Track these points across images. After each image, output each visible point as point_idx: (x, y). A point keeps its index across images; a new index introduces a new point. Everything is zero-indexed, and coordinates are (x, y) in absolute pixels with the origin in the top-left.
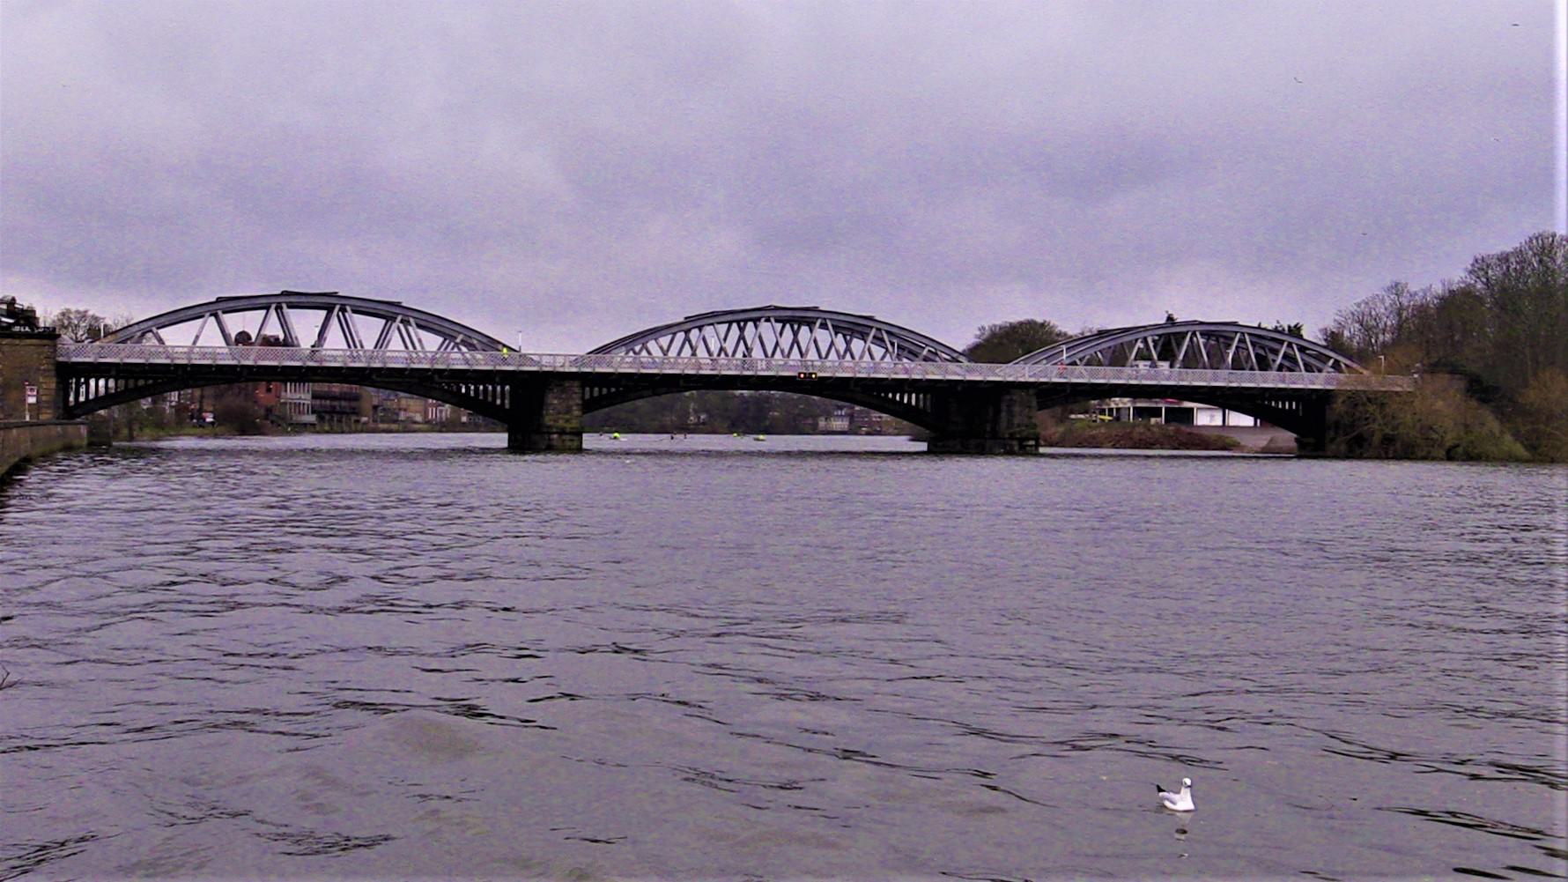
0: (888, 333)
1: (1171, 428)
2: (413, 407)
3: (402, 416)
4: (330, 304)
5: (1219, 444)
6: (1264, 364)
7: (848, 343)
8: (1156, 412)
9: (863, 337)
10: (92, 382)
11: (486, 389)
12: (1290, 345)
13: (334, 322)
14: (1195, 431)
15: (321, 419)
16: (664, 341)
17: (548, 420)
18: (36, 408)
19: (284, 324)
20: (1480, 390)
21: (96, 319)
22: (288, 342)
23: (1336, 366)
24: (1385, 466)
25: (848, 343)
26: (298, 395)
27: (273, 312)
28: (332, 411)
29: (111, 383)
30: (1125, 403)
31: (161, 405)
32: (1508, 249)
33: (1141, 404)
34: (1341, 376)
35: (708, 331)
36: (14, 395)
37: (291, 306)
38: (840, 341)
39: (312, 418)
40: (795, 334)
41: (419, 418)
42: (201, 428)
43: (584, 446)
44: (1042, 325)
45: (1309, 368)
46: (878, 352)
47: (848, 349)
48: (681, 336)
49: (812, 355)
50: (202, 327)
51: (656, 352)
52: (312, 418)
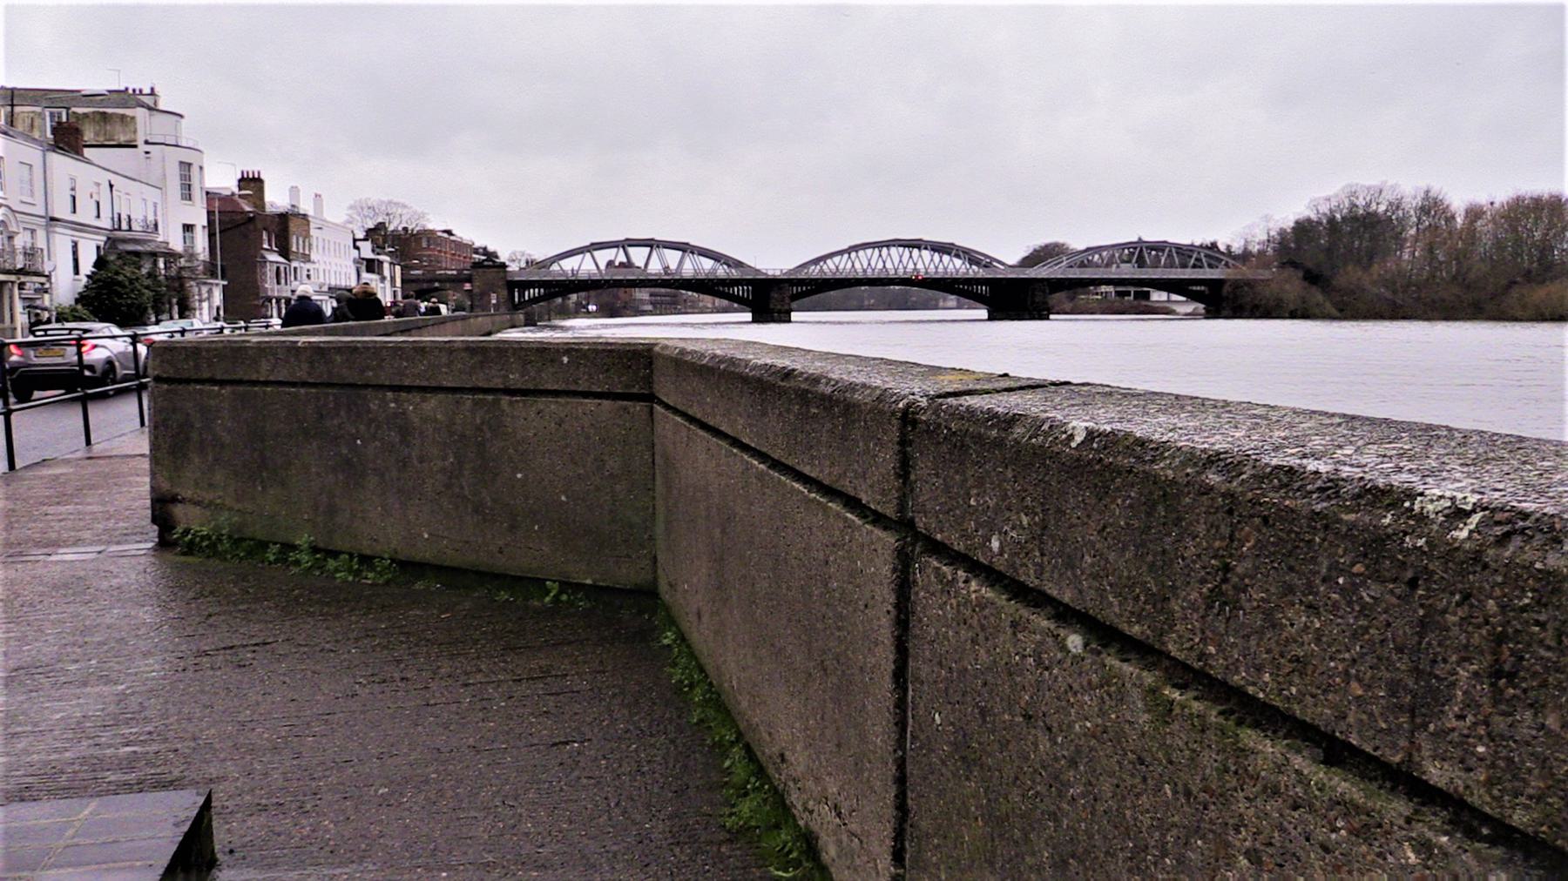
0: (963, 252)
1: (1136, 302)
2: (707, 300)
3: (701, 304)
4: (651, 244)
5: (1164, 311)
6: (1184, 266)
7: (941, 257)
8: (1128, 293)
9: (949, 254)
10: (532, 291)
11: (748, 289)
12: (1199, 253)
13: (654, 253)
14: (1149, 304)
15: (655, 307)
17: (772, 306)
18: (497, 307)
20: (1313, 278)
21: (530, 255)
22: (628, 265)
23: (1227, 265)
24: (1556, 329)
26: (642, 294)
27: (621, 250)
28: (662, 303)
29: (542, 290)
30: (1110, 289)
31: (567, 302)
32: (1331, 193)
33: (1120, 289)
34: (1229, 270)
36: (486, 298)
37: (630, 246)
39: (650, 307)
40: (911, 253)
41: (710, 305)
42: (589, 314)
43: (792, 319)
44: (1063, 245)
45: (1210, 266)
46: (958, 262)
48: (846, 256)
50: (583, 258)
52: (650, 307)
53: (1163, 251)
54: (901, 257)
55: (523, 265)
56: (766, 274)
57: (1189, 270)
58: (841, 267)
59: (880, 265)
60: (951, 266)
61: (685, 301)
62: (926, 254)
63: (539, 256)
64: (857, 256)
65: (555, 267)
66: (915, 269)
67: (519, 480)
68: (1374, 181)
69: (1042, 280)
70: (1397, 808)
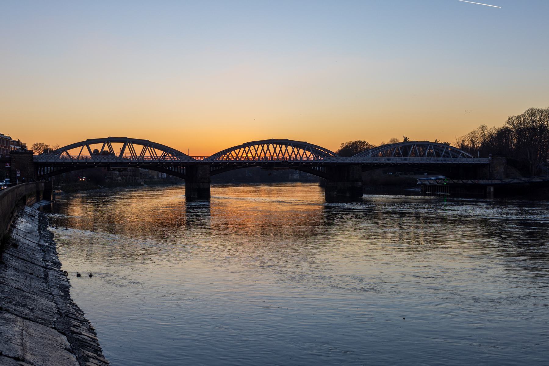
4: (126, 141)
7: (298, 151)
10: (46, 168)
11: (183, 169)
16: (237, 151)
19: (110, 147)
21: (47, 146)
22: (112, 154)
25: (298, 151)
29: (52, 168)
35: (252, 148)
38: (295, 149)
40: (281, 148)
45: (453, 156)
46: (308, 153)
47: (298, 153)
48: (242, 149)
49: (287, 155)
51: (235, 155)
54: (256, 151)
55: (42, 151)
58: (240, 155)
59: (244, 155)
60: (305, 155)
61: (141, 174)
62: (290, 149)
63: (53, 146)
65: (64, 154)
66: (283, 157)
67: (23, 178)
68: (532, 107)
69: (358, 164)
70: (173, 206)
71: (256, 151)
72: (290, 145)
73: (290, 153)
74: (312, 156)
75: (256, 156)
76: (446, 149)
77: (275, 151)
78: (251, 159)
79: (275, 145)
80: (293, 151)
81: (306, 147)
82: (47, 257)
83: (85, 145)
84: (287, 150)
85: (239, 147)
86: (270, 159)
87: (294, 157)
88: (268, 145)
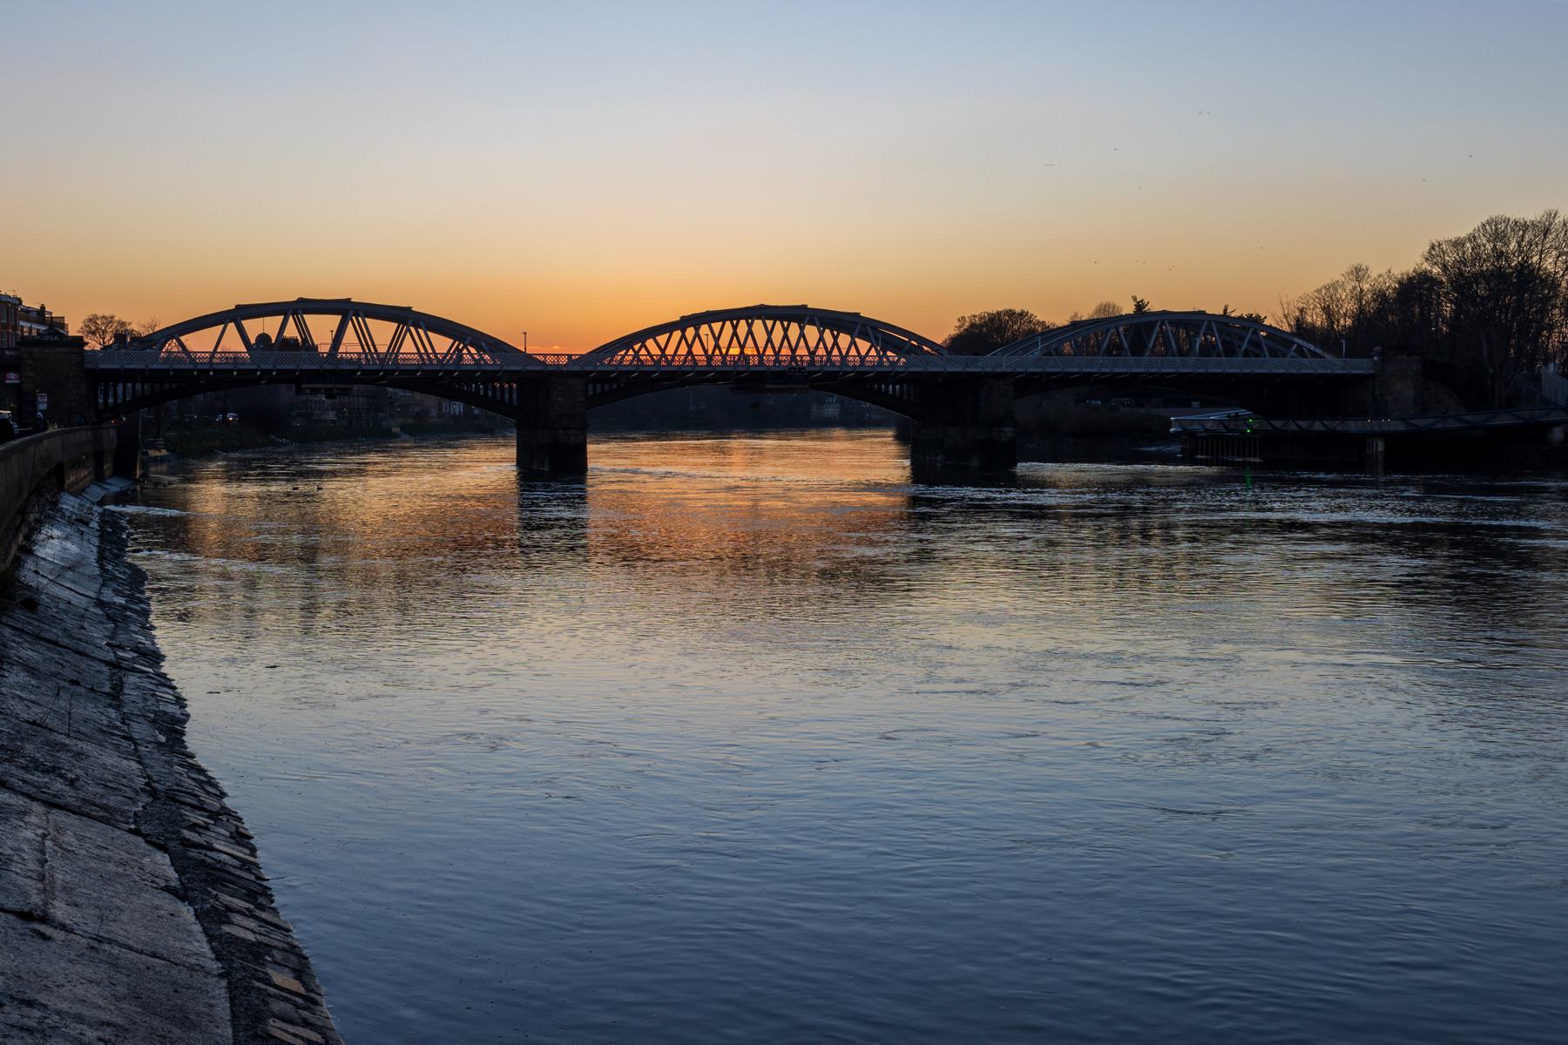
4: (346, 310)
7: (835, 338)
16: (662, 339)
19: (302, 327)
21: (123, 324)
22: (307, 345)
25: (835, 338)
32: (1463, 234)
35: (704, 329)
40: (786, 330)
45: (1274, 354)
46: (864, 346)
47: (835, 343)
48: (677, 334)
49: (802, 351)
51: (655, 351)
53: (1200, 327)
56: (544, 363)
57: (1239, 359)
58: (670, 351)
59: (683, 350)
60: (853, 352)
62: (812, 332)
63: (139, 324)
64: (697, 335)
65: (172, 346)
71: (717, 339)
72: (812, 323)
73: (761, 343)
74: (873, 352)
75: (717, 352)
76: (1253, 332)
77: (769, 340)
78: (702, 361)
79: (769, 323)
80: (821, 339)
81: (807, 318)
82: (122, 638)
83: (231, 322)
84: (802, 335)
85: (668, 328)
86: (702, 361)
87: (822, 356)
88: (750, 321)
